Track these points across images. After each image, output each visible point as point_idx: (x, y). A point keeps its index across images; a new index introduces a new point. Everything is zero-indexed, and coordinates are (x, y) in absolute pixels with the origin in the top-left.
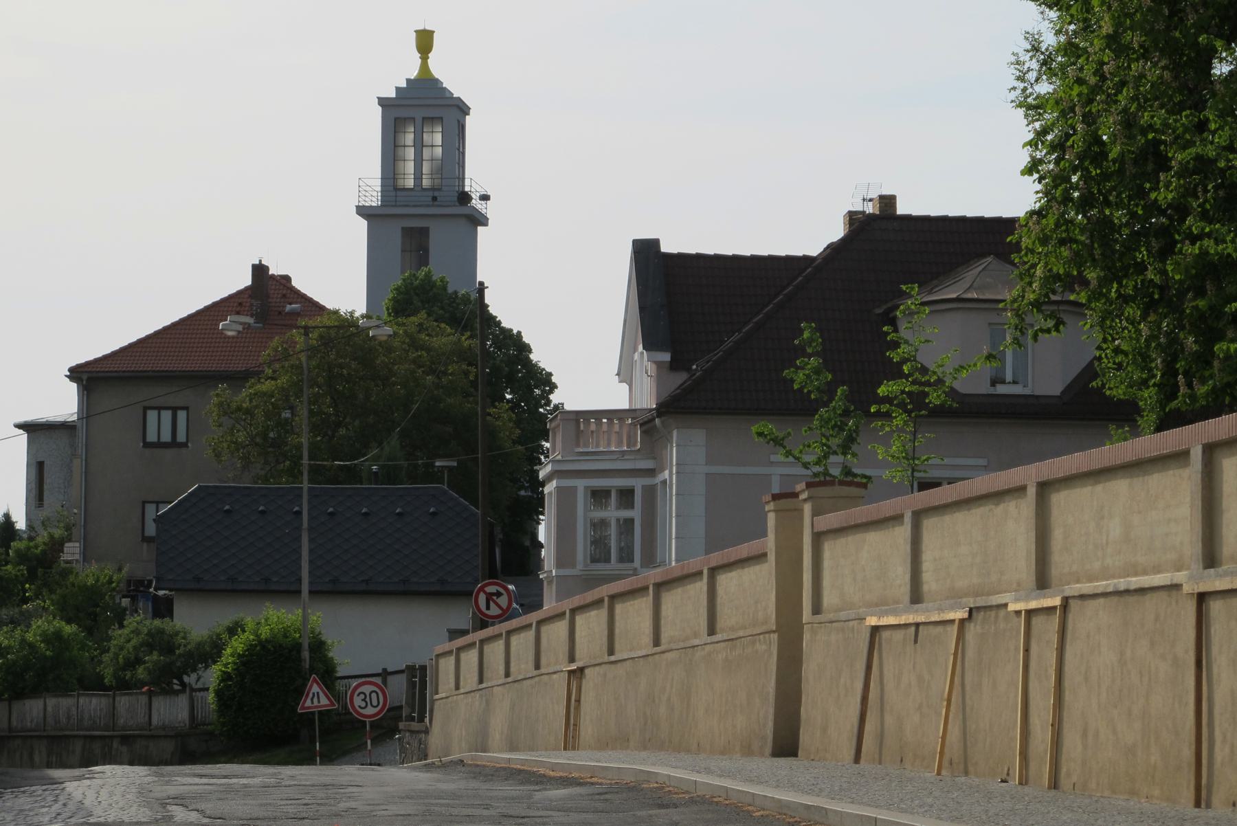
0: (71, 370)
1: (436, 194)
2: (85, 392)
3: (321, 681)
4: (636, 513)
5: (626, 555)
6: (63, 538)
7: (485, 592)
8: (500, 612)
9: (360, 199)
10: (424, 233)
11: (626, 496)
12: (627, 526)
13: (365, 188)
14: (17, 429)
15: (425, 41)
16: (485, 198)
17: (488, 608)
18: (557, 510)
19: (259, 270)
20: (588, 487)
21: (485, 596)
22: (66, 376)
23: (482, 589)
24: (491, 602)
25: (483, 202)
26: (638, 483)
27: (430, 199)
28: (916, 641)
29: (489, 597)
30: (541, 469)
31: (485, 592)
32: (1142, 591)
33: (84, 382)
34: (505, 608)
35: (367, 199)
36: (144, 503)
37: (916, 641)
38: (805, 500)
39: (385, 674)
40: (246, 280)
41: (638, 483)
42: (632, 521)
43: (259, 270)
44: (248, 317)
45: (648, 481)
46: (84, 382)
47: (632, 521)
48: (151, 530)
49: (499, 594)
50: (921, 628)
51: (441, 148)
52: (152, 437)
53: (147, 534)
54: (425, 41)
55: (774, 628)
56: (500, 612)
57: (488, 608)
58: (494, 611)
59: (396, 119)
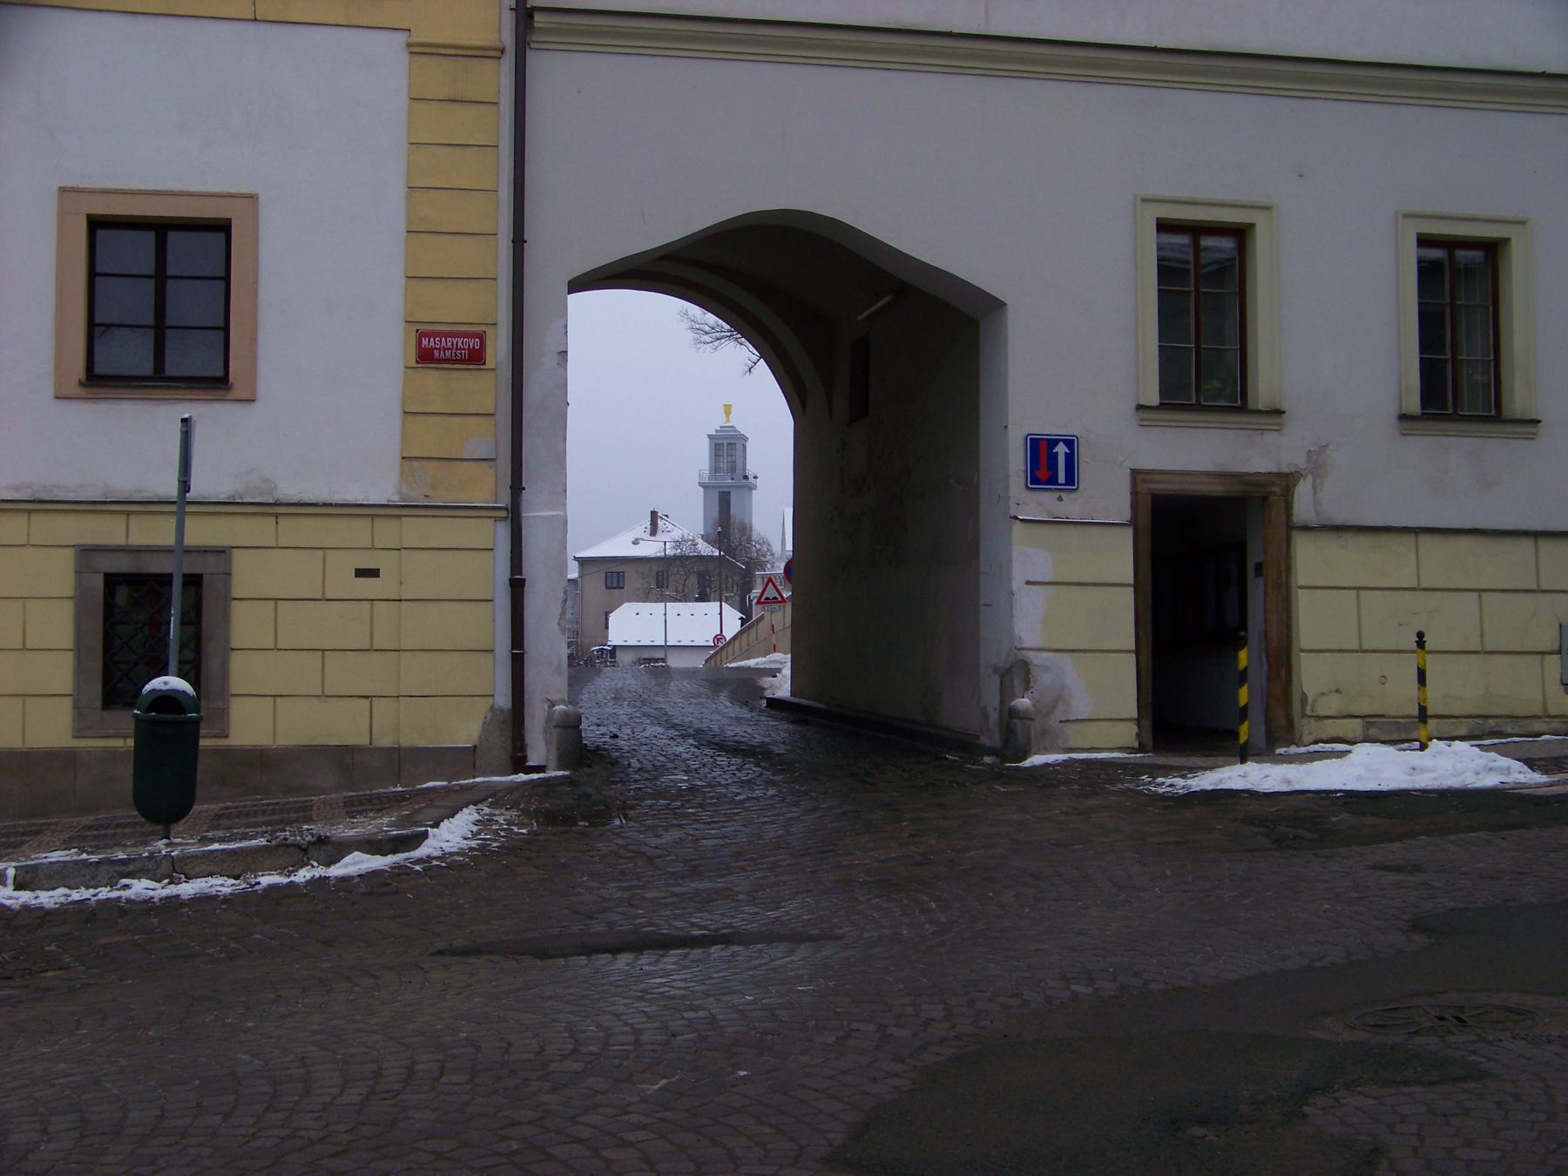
15: (728, 410)
51: (153, 280)
54: (728, 410)
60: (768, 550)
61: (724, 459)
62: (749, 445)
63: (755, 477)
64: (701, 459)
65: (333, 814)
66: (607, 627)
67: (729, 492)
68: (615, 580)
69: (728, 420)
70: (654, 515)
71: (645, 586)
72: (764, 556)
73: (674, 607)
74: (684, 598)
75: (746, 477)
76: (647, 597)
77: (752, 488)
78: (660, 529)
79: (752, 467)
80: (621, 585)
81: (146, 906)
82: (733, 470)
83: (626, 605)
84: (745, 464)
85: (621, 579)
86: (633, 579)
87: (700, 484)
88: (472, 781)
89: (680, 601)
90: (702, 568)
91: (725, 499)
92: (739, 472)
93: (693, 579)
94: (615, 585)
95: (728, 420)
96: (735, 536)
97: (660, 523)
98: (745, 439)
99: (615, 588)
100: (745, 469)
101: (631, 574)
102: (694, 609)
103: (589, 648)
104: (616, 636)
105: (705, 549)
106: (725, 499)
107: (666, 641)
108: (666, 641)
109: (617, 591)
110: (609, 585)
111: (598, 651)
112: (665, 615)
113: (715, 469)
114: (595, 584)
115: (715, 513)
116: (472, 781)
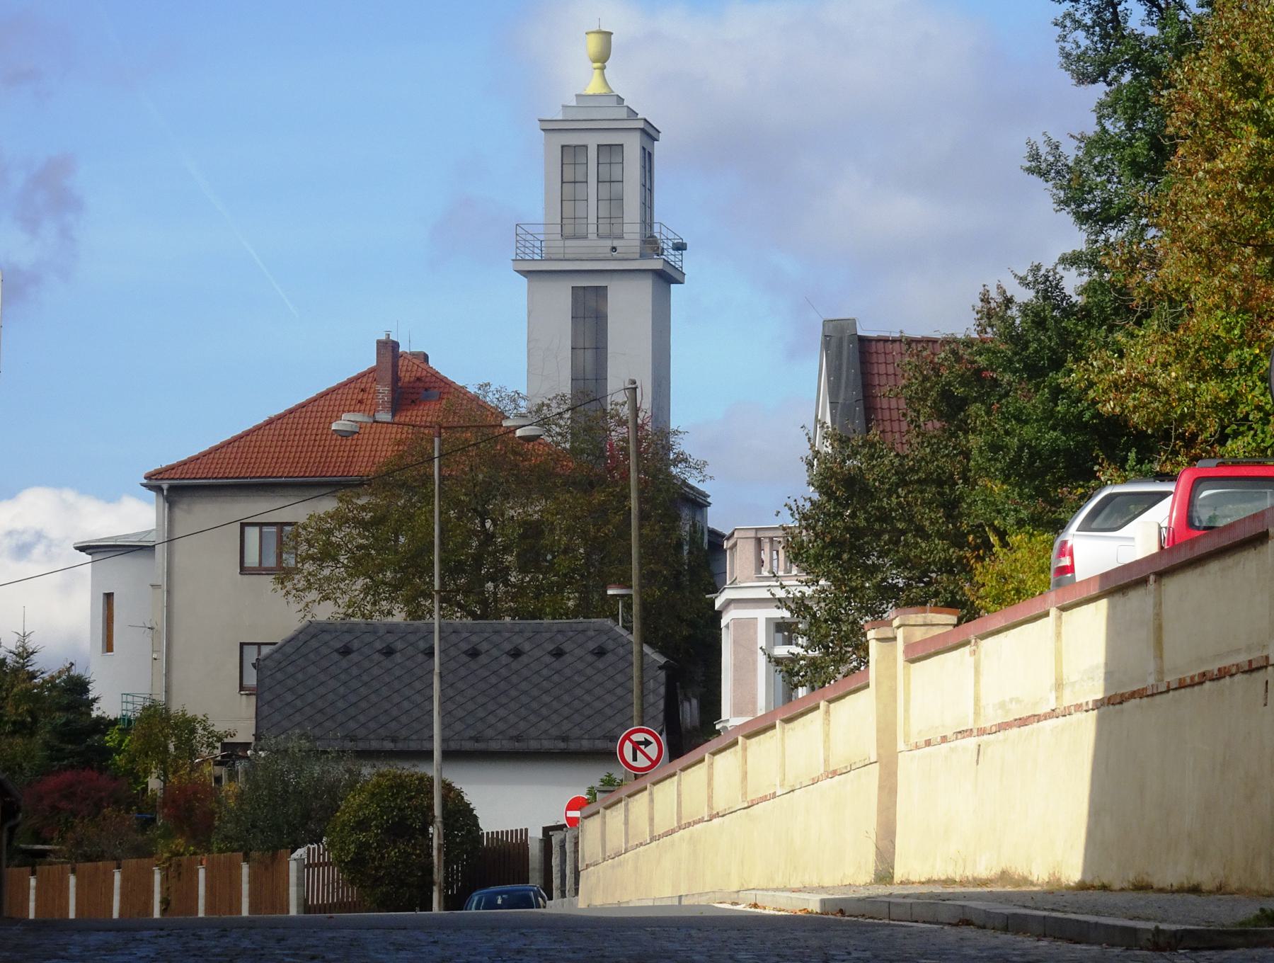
0: (148, 477)
1: (616, 243)
2: (167, 505)
6: (130, 721)
7: (631, 741)
8: (649, 763)
9: (518, 251)
10: (601, 292)
13: (524, 236)
14: (78, 551)
16: (680, 247)
17: (635, 759)
19: (388, 348)
20: (770, 618)
21: (631, 745)
22: (143, 485)
23: (627, 737)
24: (638, 751)
25: (677, 253)
27: (608, 250)
29: (636, 746)
30: (716, 597)
31: (631, 741)
33: (165, 492)
34: (654, 758)
35: (527, 251)
36: (242, 645)
38: (898, 627)
40: (368, 360)
43: (388, 348)
44: (361, 414)
46: (165, 492)
48: (251, 679)
49: (647, 743)
52: (252, 559)
53: (245, 683)
56: (649, 763)
57: (635, 759)
58: (642, 762)
59: (563, 147)
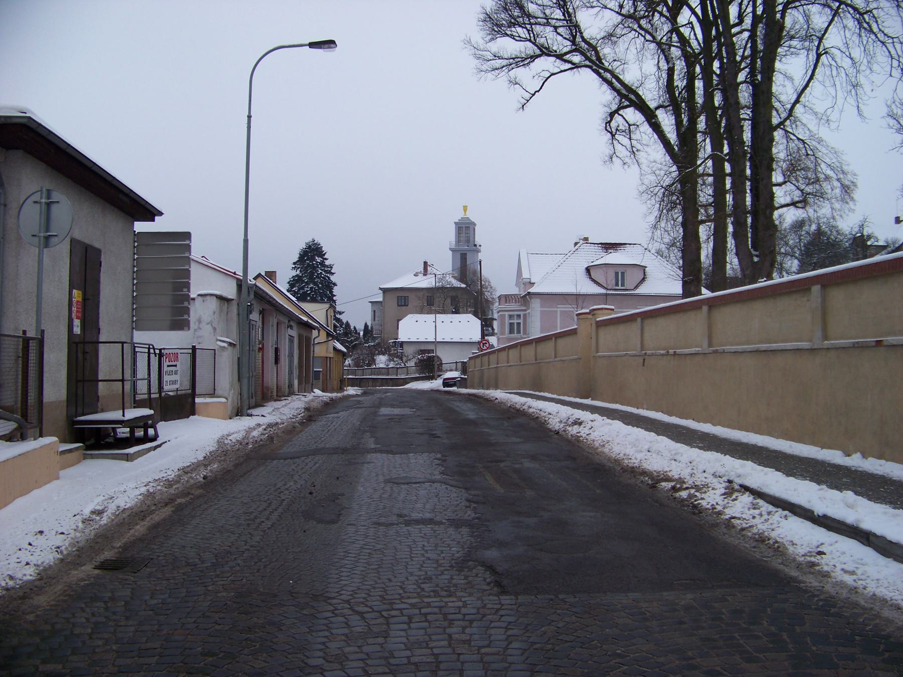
3: (898, 336)
4: (521, 321)
5: (519, 332)
11: (519, 316)
12: (519, 324)
15: (465, 208)
18: (843, 270)
26: (522, 313)
28: (643, 365)
32: (774, 351)
37: (643, 365)
39: (456, 362)
41: (522, 313)
42: (520, 323)
45: (524, 313)
47: (520, 323)
50: (121, 383)
51: (100, 378)
54: (465, 208)
55: (100, 383)
58: (485, 348)
60: (489, 285)
61: (463, 235)
62: (476, 228)
63: (480, 246)
64: (450, 236)
65: (673, 194)
66: (398, 329)
67: (466, 254)
68: (403, 300)
69: (465, 214)
70: (425, 263)
71: (421, 305)
72: (487, 288)
73: (441, 317)
74: (444, 312)
75: (475, 245)
76: (422, 309)
77: (478, 251)
78: (429, 272)
79: (478, 240)
80: (407, 304)
81: (722, 27)
82: (468, 241)
83: (410, 316)
84: (474, 238)
85: (407, 300)
86: (413, 301)
87: (450, 249)
88: (750, 240)
89: (442, 313)
90: (454, 294)
91: (464, 257)
92: (471, 243)
93: (449, 301)
94: (403, 304)
95: (465, 214)
96: (470, 276)
97: (429, 268)
98: (474, 224)
99: (403, 306)
100: (474, 241)
101: (412, 297)
102: (452, 318)
103: (388, 341)
104: (403, 336)
105: (457, 284)
106: (464, 257)
107: (436, 339)
108: (436, 339)
109: (404, 308)
110: (400, 304)
111: (393, 343)
112: (435, 322)
113: (458, 241)
114: (392, 303)
115: (458, 265)
116: (750, 240)
